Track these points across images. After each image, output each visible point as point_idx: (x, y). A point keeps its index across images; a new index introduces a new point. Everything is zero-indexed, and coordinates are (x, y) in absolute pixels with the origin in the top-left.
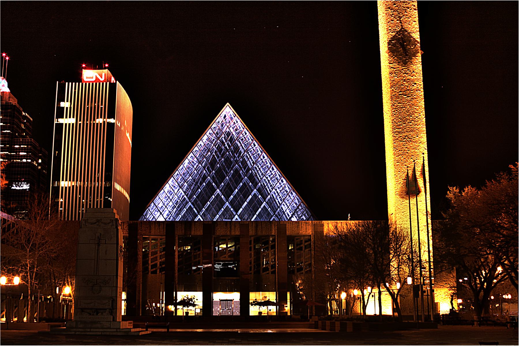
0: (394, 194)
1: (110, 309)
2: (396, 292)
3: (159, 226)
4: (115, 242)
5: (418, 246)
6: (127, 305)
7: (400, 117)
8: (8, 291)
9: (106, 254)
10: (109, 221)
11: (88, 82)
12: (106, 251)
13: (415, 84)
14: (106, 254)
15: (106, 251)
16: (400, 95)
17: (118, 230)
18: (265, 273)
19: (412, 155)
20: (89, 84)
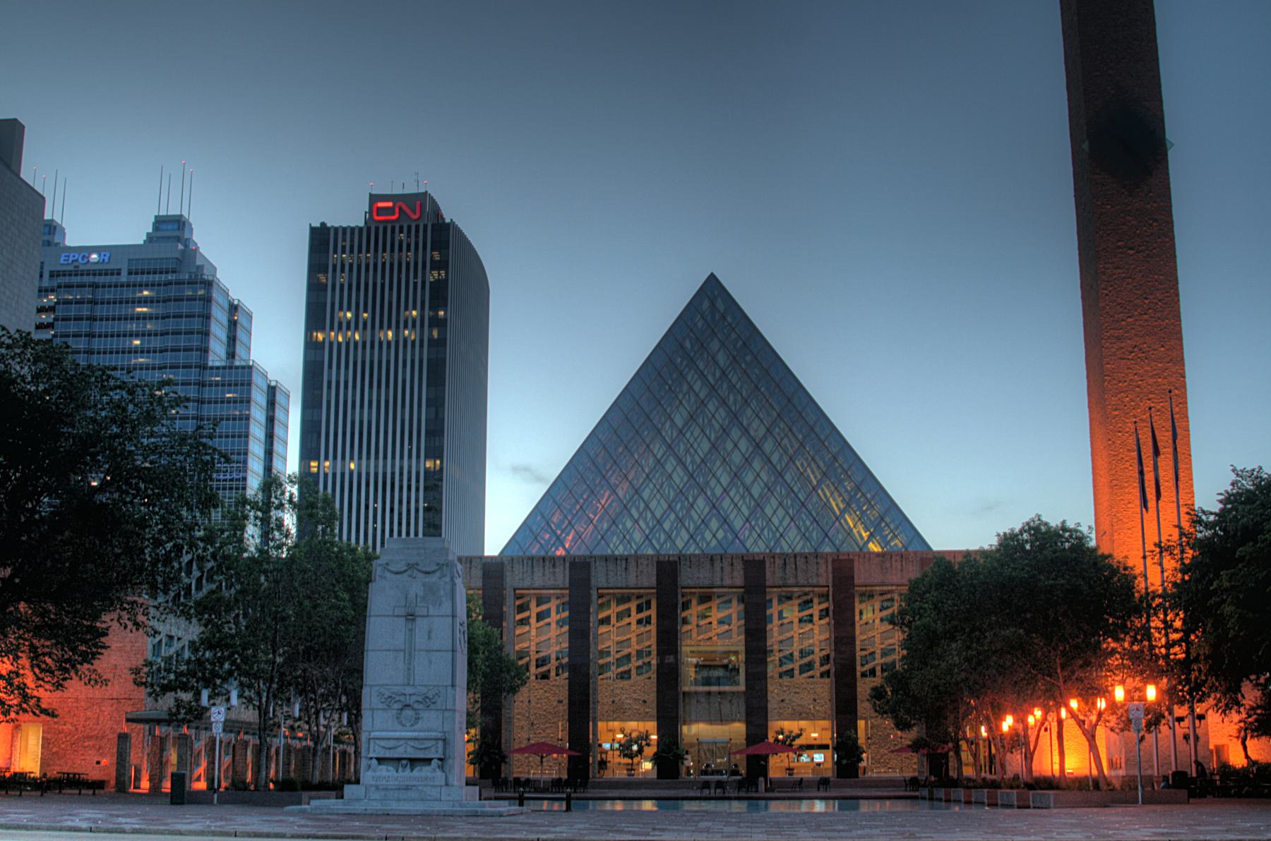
0: (1027, 520)
1: (440, 759)
2: (1186, 706)
3: (554, 566)
4: (449, 612)
5: (394, 806)
6: (746, 612)
7: (1119, 300)
8: (7, 581)
9: (429, 638)
10: (435, 568)
11: (381, 221)
12: (430, 632)
13: (1156, 220)
14: (429, 638)
15: (430, 632)
16: (1119, 247)
17: (454, 585)
18: (805, 675)
19: (1151, 393)
20: (385, 229)
